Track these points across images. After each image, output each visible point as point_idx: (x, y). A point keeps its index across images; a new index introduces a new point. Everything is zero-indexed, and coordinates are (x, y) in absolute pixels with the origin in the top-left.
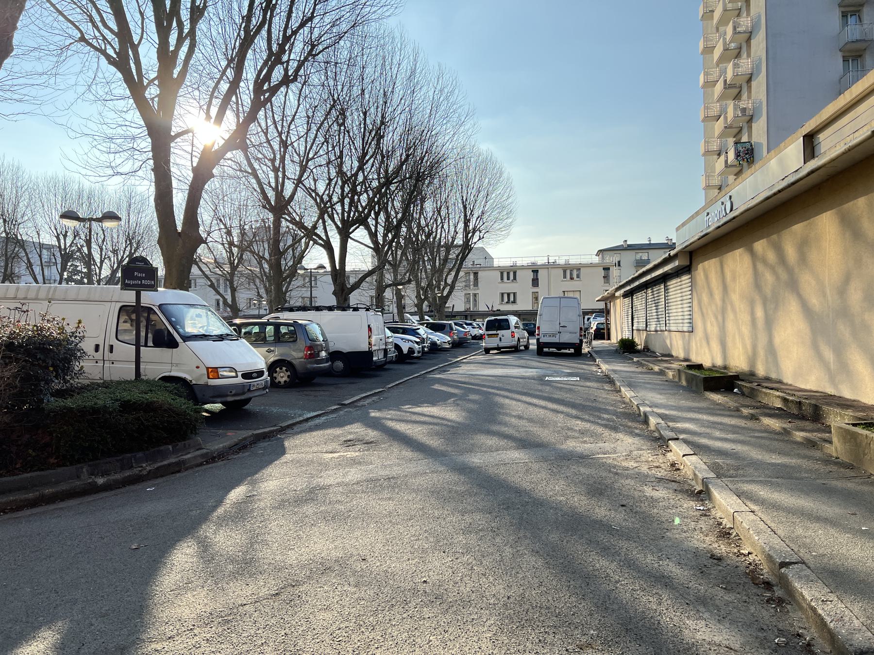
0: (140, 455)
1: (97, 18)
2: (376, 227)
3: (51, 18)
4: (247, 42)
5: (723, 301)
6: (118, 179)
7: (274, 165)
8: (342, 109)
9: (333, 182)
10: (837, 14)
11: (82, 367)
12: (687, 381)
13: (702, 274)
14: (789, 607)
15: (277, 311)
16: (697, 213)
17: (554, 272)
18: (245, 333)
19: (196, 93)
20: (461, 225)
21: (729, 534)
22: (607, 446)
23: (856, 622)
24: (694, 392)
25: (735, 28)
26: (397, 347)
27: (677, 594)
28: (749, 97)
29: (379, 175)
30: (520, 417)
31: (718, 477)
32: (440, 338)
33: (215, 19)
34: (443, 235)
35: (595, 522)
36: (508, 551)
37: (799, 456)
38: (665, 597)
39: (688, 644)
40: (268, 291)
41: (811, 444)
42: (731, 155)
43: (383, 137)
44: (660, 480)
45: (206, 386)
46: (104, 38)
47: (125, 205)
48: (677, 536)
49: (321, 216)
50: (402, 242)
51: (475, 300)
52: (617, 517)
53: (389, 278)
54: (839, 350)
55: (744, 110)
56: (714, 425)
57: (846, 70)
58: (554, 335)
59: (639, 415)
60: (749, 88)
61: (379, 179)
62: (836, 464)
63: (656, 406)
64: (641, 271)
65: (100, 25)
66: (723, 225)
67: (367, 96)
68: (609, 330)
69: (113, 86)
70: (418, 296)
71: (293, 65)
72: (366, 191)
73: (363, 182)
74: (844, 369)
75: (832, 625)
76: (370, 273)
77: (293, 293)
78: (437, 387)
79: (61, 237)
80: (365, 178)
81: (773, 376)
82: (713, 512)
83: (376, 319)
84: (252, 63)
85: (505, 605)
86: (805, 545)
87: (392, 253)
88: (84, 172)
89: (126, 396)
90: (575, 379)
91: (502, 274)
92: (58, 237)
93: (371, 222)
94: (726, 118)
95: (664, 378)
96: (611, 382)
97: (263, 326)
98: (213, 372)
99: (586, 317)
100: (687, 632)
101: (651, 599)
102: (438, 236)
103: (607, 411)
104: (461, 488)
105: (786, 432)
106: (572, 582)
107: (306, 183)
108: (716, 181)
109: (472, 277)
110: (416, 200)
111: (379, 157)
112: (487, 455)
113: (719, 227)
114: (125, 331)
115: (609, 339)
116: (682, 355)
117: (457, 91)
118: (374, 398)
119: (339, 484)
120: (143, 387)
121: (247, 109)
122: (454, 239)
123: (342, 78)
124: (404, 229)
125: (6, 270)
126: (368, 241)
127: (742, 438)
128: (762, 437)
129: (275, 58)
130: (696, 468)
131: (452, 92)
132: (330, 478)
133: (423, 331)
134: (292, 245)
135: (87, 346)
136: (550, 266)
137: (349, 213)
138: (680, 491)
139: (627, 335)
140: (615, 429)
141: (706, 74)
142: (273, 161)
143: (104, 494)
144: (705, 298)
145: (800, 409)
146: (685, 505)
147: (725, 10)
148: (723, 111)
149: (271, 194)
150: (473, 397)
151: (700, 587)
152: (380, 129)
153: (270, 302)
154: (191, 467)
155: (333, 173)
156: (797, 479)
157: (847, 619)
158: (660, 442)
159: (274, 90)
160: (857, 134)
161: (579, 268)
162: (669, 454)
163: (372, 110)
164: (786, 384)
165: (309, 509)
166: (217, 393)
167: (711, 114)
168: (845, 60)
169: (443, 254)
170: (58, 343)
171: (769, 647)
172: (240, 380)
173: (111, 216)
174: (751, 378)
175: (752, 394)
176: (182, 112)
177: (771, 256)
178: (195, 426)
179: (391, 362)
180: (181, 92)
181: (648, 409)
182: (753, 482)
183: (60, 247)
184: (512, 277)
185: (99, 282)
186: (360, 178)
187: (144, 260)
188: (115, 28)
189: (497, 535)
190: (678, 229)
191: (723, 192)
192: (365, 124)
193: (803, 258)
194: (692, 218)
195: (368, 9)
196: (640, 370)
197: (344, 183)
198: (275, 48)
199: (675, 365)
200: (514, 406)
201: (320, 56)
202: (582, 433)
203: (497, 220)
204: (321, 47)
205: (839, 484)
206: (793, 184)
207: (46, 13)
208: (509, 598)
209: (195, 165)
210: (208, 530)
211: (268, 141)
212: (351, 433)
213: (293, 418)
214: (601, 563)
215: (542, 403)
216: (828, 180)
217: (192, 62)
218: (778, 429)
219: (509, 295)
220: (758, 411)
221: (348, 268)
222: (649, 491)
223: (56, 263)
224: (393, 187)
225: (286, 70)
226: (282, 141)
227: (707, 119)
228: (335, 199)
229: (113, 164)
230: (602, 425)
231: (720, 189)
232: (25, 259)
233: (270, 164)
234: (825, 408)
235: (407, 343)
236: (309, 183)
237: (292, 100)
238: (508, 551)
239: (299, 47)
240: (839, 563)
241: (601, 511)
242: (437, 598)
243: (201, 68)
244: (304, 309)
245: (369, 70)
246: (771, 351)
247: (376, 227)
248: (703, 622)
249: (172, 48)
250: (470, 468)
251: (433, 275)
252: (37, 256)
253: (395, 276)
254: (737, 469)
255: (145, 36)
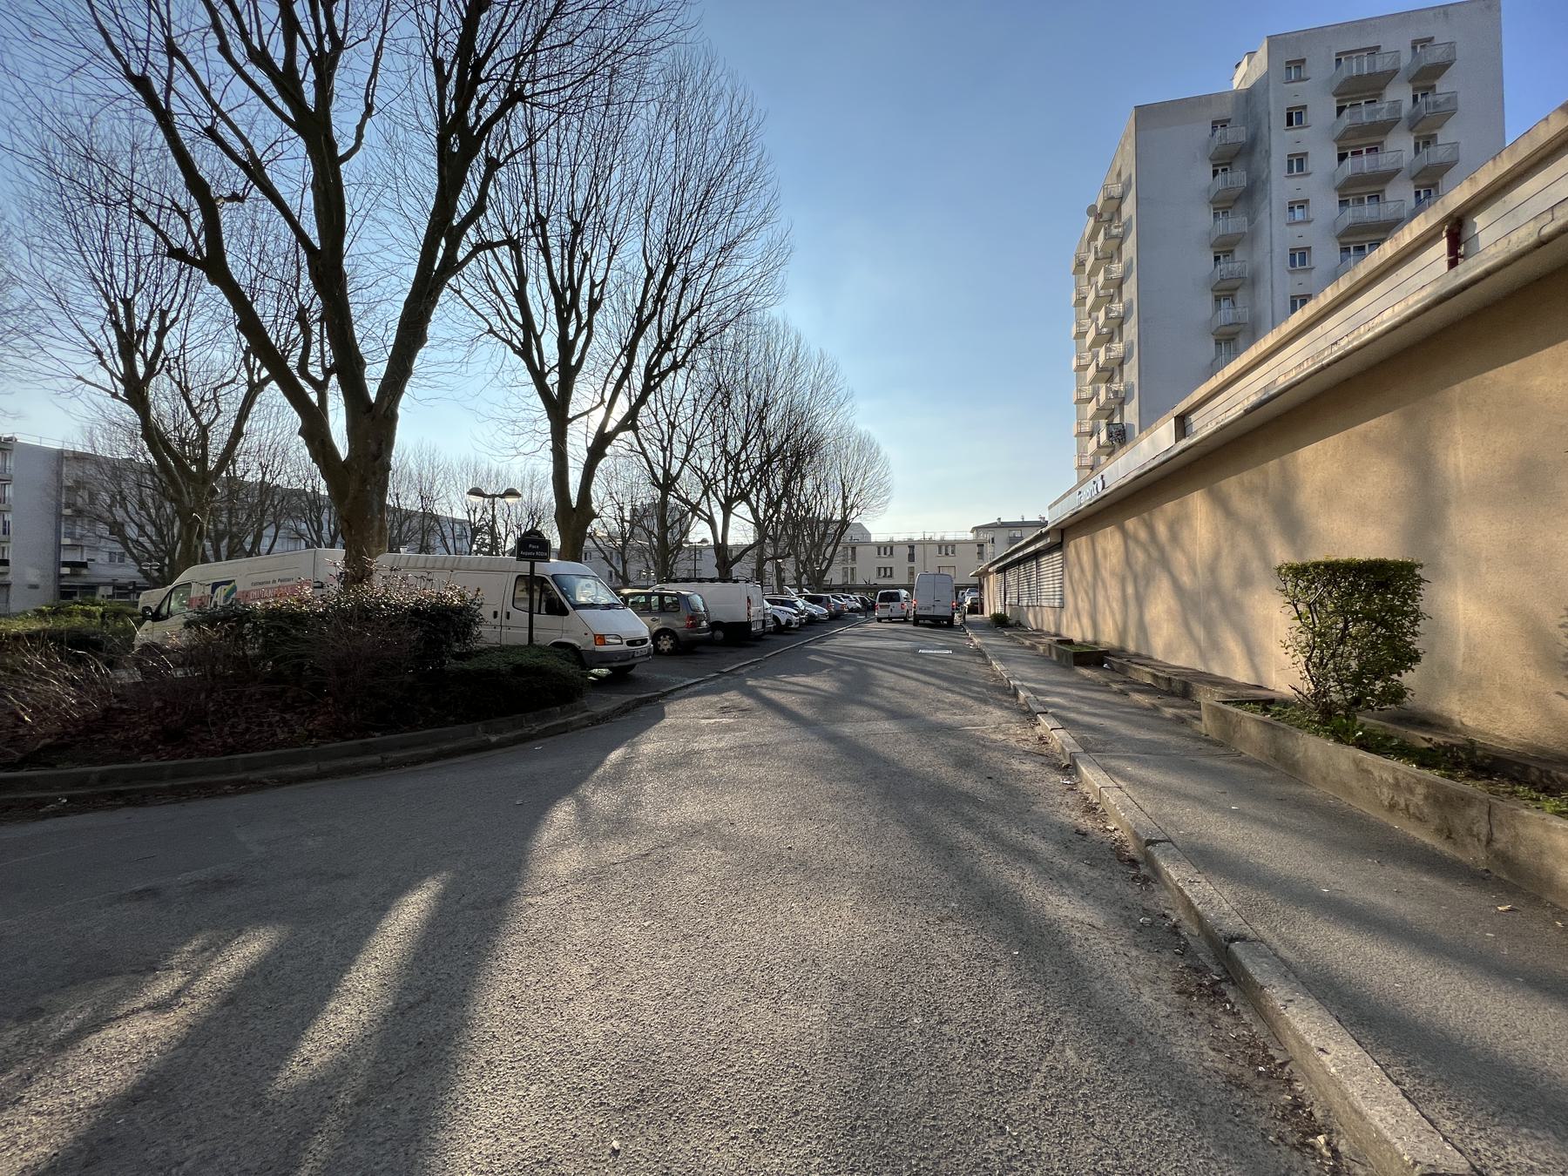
0: (530, 715)
1: (504, 311)
2: (757, 502)
3: (464, 312)
4: (640, 330)
5: (1095, 578)
6: (521, 458)
7: (662, 446)
8: (727, 392)
9: (717, 461)
10: (1210, 298)
11: (480, 632)
12: (1058, 656)
13: (1073, 551)
14: (1154, 885)
15: (662, 582)
16: (1070, 492)
17: (929, 548)
18: (632, 603)
19: (592, 378)
20: (840, 502)
21: (1095, 809)
22: (977, 719)
23: (1226, 907)
24: (1064, 667)
25: (1106, 314)
26: (775, 618)
27: (1040, 869)
28: (1121, 380)
29: (760, 454)
30: (893, 689)
31: (1086, 751)
32: (815, 609)
33: (611, 310)
34: (822, 510)
35: (962, 793)
36: (873, 820)
37: (1168, 732)
38: (1028, 871)
39: (1050, 920)
40: (655, 564)
41: (1180, 720)
42: (1103, 436)
43: (765, 418)
44: (1027, 753)
45: (594, 652)
46: (511, 331)
47: (528, 482)
48: (1043, 810)
49: (705, 493)
50: (782, 517)
51: (852, 574)
52: (984, 790)
53: (769, 552)
54: (1209, 626)
55: (1116, 393)
56: (1082, 700)
57: (1218, 353)
58: (929, 608)
59: (1009, 688)
60: (1121, 371)
61: (761, 457)
62: (1206, 741)
63: (1026, 680)
64: (1013, 548)
65: (507, 317)
66: (1094, 503)
67: (750, 380)
68: (982, 604)
69: (519, 373)
70: (797, 570)
71: (682, 351)
72: (749, 469)
73: (746, 461)
74: (1216, 645)
75: (1200, 907)
76: (750, 547)
77: (680, 566)
78: (812, 657)
79: (471, 513)
80: (748, 457)
81: (1144, 652)
82: (1080, 786)
83: (754, 590)
84: (644, 350)
85: (867, 874)
86: (1172, 823)
87: (773, 528)
88: (491, 452)
89: (519, 660)
90: (947, 652)
91: (879, 548)
92: (468, 512)
93: (753, 497)
94: (1098, 400)
95: (1035, 652)
96: (984, 656)
97: (649, 596)
98: (601, 639)
99: (961, 592)
100: (1049, 907)
101: (1014, 873)
102: (817, 511)
103: (977, 684)
104: (830, 757)
105: (1156, 708)
106: (935, 854)
107: (692, 461)
108: (1088, 461)
109: (850, 552)
110: (796, 478)
111: (762, 437)
112: (858, 725)
113: (1090, 505)
114: (520, 599)
115: (982, 613)
116: (1053, 630)
117: (836, 376)
118: (752, 667)
119: (713, 749)
120: (534, 652)
121: (638, 393)
122: (832, 515)
123: (726, 364)
124: (784, 506)
125: (422, 542)
126: (750, 516)
127: (1110, 713)
128: (1131, 713)
129: (664, 346)
130: (1063, 741)
131: (832, 376)
132: (705, 743)
133: (800, 603)
134: (679, 520)
135: (486, 612)
136: (923, 543)
137: (732, 490)
138: (1047, 765)
139: (999, 610)
140: (985, 702)
141: (1079, 358)
142: (661, 441)
143: (498, 751)
144: (1076, 574)
145: (1170, 685)
146: (1052, 779)
147: (1097, 296)
148: (1096, 393)
149: (659, 473)
150: (847, 668)
151: (1063, 863)
152: (762, 410)
153: (658, 574)
154: (578, 728)
155: (718, 451)
156: (1165, 755)
157: (1215, 902)
158: (1029, 716)
159: (663, 375)
160: (1229, 413)
161: (953, 544)
162: (1037, 728)
163: (755, 393)
164: (1156, 661)
165: (683, 774)
166: (603, 659)
167: (1084, 396)
168: (1218, 343)
169: (822, 529)
170: (458, 611)
171: (1133, 927)
172: (625, 647)
173: (511, 493)
174: (1122, 654)
175: (1122, 670)
176: (579, 396)
177: (1143, 534)
178: (581, 689)
179: (770, 633)
180: (579, 377)
181: (1018, 683)
182: (1119, 757)
183: (470, 521)
184: (888, 553)
185: (504, 554)
186: (743, 457)
187: (539, 534)
188: (520, 320)
189: (864, 804)
190: (1050, 507)
191: (1095, 472)
192: (749, 406)
193: (1174, 538)
194: (1064, 496)
195: (752, 299)
196: (1011, 644)
197: (727, 462)
198: (665, 336)
199: (1046, 640)
200: (888, 678)
201: (708, 342)
202: (952, 704)
203: (874, 497)
204: (708, 334)
205: (1209, 762)
206: (1164, 462)
207: (458, 307)
208: (872, 867)
209: (589, 445)
210: (586, 790)
211: (657, 423)
212: (727, 700)
213: (674, 684)
214: (965, 836)
215: (914, 675)
216: (1198, 460)
217: (589, 350)
218: (1148, 705)
219: (885, 569)
220: (1127, 686)
221: (730, 542)
222: (1015, 764)
223: (466, 537)
224: (774, 465)
225: (675, 357)
226: (670, 422)
227: (1079, 401)
228: (719, 477)
229: (517, 446)
230: (972, 698)
231: (1092, 469)
232: (439, 532)
233: (658, 444)
234: (1195, 685)
235: (785, 614)
236: (695, 461)
237: (680, 384)
238: (873, 820)
239: (687, 335)
240: (1207, 842)
241: (968, 783)
242: (802, 865)
243: (597, 356)
244: (687, 580)
245: (753, 355)
246: (1142, 627)
247: (757, 502)
248: (1066, 898)
249: (571, 338)
250: (839, 737)
251: (812, 550)
252: (450, 530)
253: (776, 551)
254: (1106, 744)
255: (548, 327)
